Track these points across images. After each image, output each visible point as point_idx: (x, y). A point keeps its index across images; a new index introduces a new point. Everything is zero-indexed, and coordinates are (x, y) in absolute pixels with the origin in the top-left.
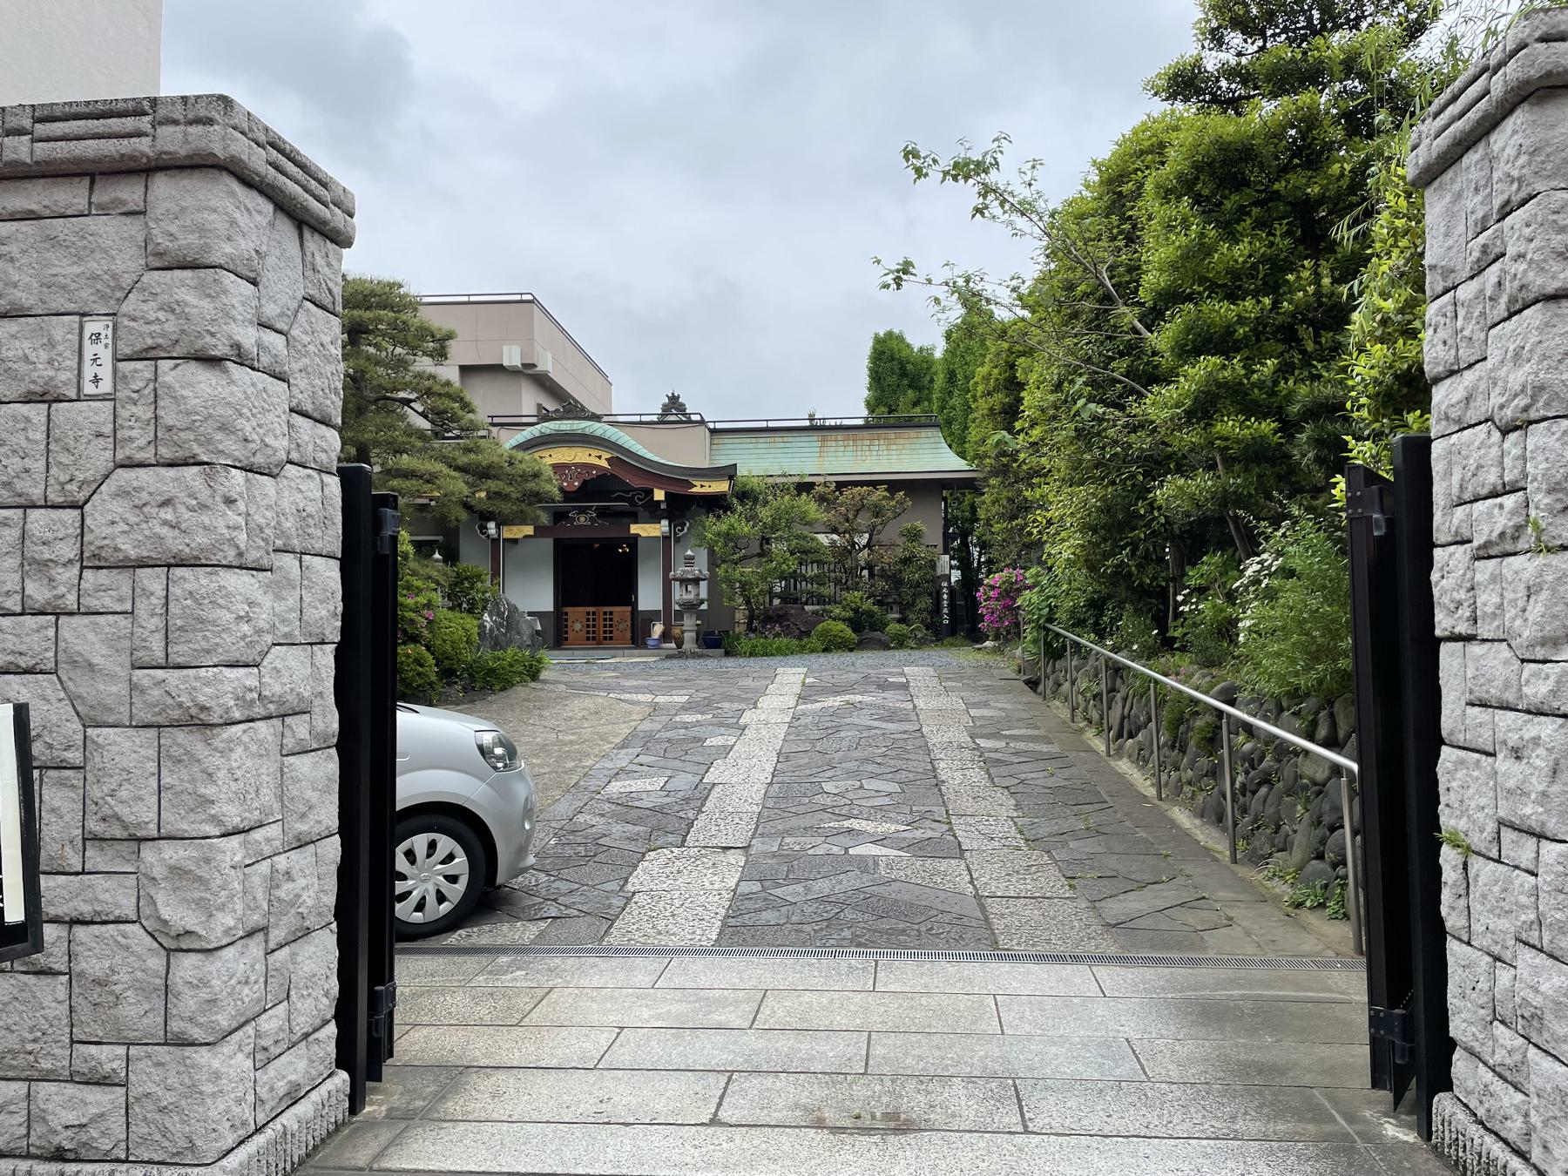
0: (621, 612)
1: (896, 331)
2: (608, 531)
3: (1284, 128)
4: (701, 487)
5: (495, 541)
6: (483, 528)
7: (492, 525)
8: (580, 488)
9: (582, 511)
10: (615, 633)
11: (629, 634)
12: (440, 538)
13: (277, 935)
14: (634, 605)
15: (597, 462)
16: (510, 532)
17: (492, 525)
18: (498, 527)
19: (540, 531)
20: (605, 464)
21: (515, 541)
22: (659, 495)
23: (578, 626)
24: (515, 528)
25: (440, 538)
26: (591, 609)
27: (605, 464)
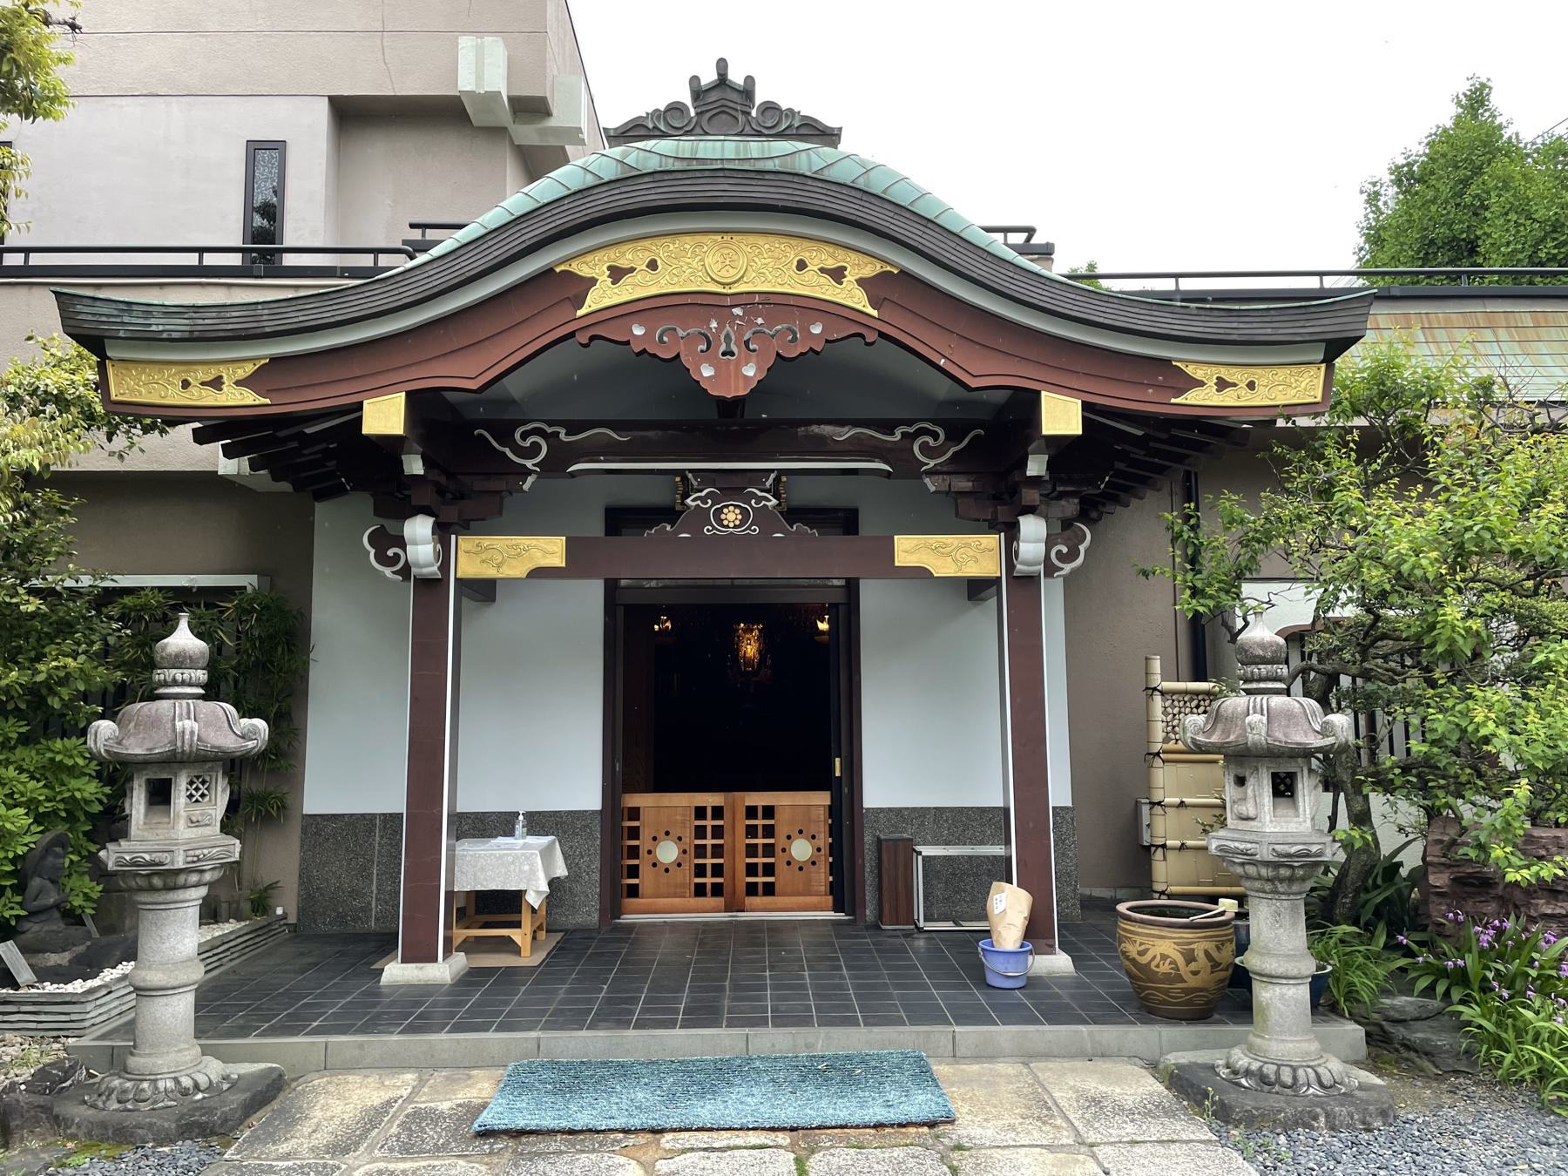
0: (801, 809)
1: (1401, 161)
2: (806, 562)
3: (653, 612)
4: (1216, 388)
5: (430, 588)
6: (389, 542)
7: (419, 530)
8: (762, 389)
9: (732, 487)
10: (781, 878)
11: (822, 877)
12: (248, 581)
13: (1419, 1159)
14: (846, 794)
15: (827, 290)
16: (478, 556)
17: (419, 530)
18: (443, 532)
19: (579, 562)
20: (857, 299)
21: (483, 591)
22: (1061, 416)
23: (668, 852)
24: (500, 543)
25: (248, 581)
26: (710, 800)
27: (857, 299)
